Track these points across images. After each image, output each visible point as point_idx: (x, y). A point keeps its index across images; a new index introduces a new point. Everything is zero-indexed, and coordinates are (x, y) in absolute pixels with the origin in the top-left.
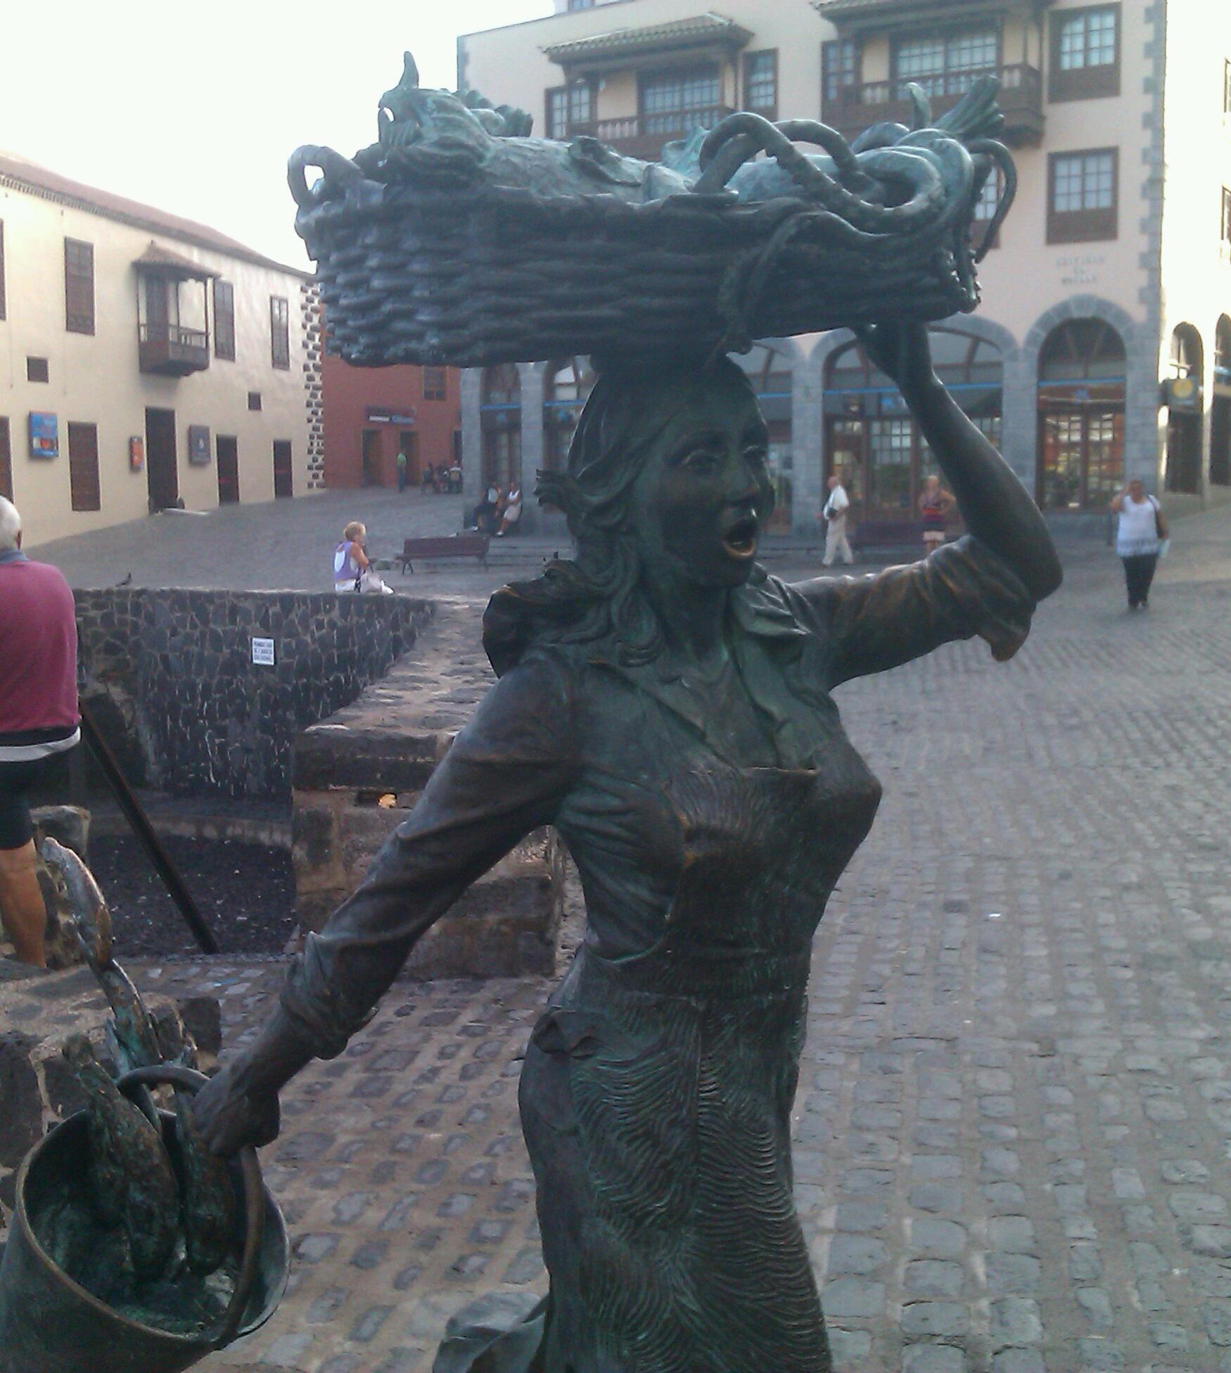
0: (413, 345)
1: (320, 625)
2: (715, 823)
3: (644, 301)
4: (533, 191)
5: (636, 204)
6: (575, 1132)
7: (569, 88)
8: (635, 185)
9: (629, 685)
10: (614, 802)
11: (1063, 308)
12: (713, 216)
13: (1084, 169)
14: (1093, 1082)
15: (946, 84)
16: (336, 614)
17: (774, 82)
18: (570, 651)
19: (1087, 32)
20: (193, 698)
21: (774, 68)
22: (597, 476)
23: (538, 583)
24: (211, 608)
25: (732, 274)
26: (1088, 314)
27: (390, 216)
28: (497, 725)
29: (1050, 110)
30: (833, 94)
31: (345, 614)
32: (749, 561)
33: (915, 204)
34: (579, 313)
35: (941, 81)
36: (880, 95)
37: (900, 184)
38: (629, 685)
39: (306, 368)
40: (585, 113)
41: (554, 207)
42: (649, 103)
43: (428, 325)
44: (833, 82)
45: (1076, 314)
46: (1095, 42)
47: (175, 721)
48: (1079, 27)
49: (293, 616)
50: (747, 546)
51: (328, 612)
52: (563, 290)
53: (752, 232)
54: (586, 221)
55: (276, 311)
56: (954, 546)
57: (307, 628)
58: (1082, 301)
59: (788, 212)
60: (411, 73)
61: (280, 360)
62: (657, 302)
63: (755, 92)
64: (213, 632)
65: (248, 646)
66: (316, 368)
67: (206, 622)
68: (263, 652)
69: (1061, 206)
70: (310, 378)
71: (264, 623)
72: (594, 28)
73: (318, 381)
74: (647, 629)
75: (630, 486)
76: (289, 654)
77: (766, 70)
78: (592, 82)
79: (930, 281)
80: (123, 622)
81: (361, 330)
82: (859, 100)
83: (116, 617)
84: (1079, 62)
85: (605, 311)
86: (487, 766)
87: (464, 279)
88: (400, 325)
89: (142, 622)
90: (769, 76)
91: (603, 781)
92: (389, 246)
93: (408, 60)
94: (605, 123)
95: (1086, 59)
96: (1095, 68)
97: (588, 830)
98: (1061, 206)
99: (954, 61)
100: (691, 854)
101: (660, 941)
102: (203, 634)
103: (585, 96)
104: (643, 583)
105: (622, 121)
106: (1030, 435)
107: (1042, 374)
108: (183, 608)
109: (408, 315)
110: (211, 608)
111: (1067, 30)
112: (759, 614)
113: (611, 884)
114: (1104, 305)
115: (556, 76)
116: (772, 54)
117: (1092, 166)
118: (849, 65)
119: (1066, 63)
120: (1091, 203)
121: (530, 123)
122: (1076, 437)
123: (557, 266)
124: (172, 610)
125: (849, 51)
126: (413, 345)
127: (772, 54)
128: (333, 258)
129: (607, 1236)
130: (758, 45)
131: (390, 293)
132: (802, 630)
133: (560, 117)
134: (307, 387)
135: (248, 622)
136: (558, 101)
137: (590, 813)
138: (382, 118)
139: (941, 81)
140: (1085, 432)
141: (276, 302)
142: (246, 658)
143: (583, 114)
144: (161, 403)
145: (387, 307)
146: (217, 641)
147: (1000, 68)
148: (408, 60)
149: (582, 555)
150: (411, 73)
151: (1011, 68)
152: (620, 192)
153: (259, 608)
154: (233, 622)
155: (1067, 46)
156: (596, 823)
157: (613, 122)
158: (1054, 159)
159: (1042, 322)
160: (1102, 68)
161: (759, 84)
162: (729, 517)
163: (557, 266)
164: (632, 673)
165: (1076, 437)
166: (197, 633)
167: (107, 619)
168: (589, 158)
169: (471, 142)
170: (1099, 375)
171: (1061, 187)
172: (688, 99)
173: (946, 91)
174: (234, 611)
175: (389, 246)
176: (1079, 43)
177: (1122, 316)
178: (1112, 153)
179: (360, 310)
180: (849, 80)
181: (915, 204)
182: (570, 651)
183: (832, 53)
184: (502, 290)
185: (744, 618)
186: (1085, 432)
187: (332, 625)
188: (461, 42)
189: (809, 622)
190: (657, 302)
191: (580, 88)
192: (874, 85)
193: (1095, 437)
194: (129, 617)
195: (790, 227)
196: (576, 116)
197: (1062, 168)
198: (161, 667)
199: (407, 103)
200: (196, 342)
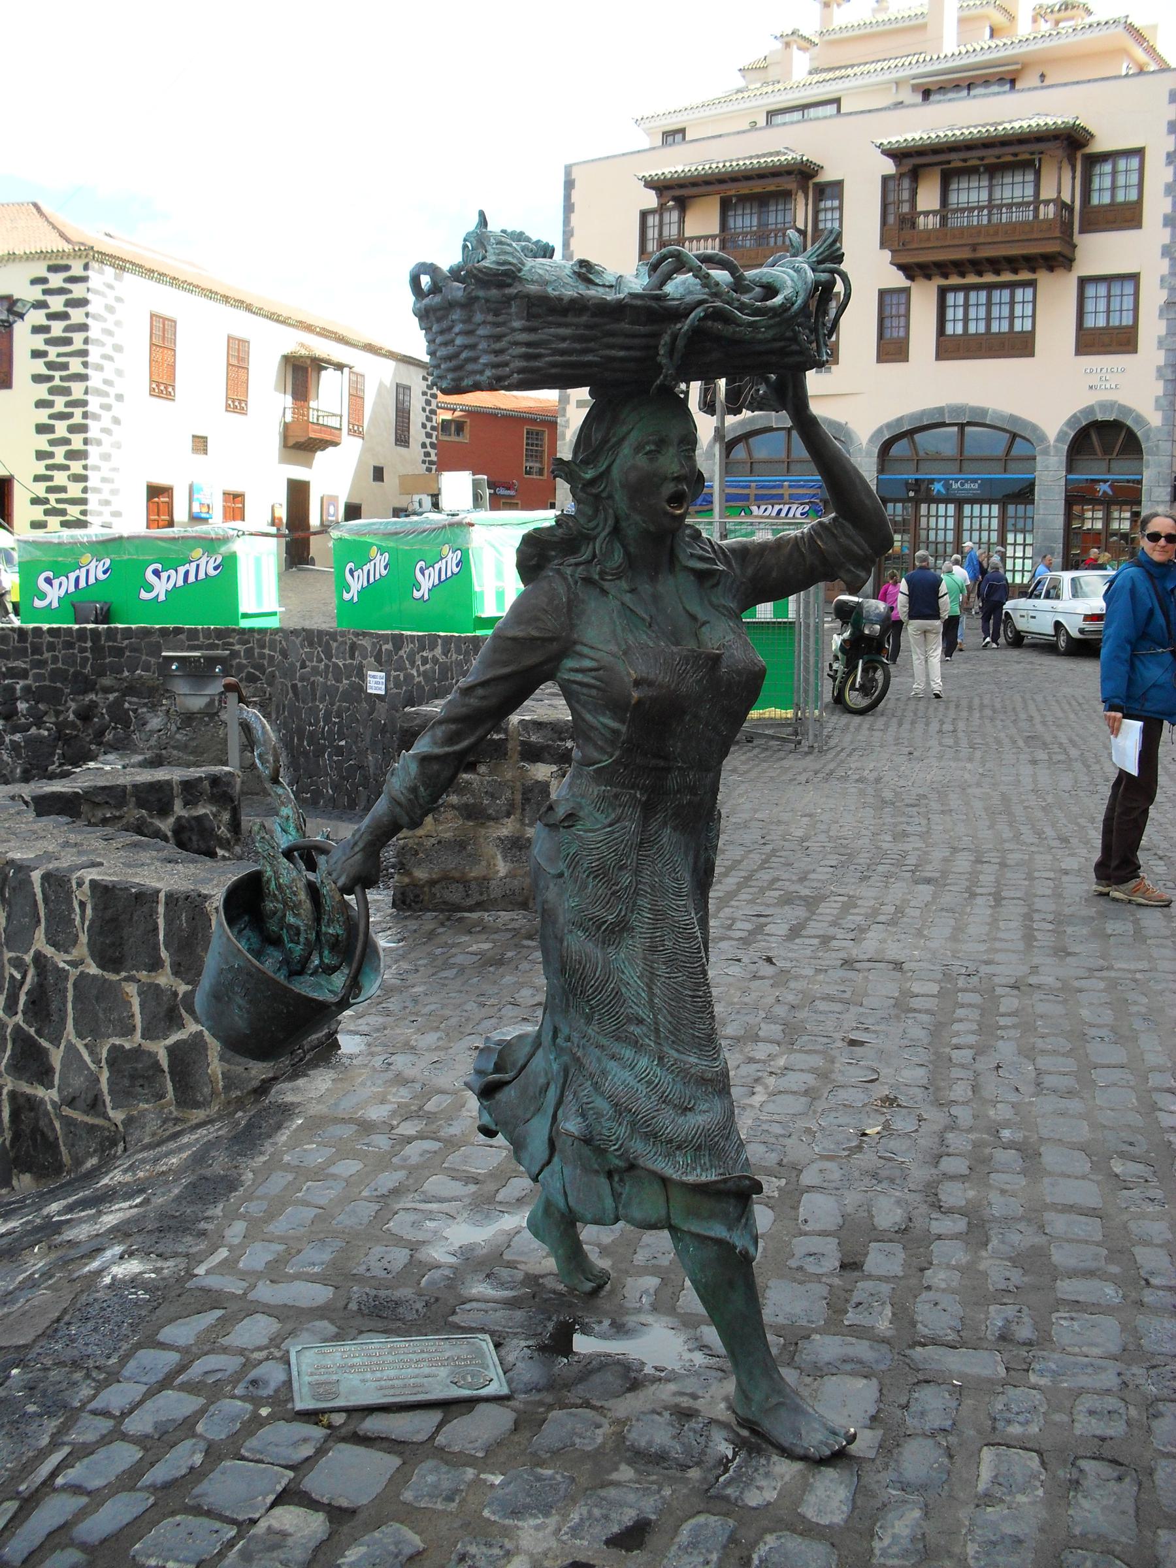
0: (478, 377)
1: (425, 661)
2: (652, 676)
3: (613, 353)
4: (550, 290)
5: (611, 296)
6: (561, 875)
7: (661, 209)
8: (611, 286)
9: (604, 592)
10: (587, 663)
11: (1090, 410)
12: (654, 304)
13: (1109, 291)
14: (999, 991)
15: (990, 214)
16: (438, 651)
17: (841, 208)
18: (569, 571)
19: (1114, 173)
20: (317, 721)
21: (840, 197)
22: (586, 462)
23: (551, 528)
24: (334, 645)
25: (666, 338)
26: (1111, 418)
27: (468, 304)
28: (519, 609)
29: (1078, 238)
30: (891, 219)
31: (446, 653)
32: (682, 517)
33: (778, 300)
34: (573, 358)
35: (985, 212)
36: (932, 222)
37: (771, 290)
38: (604, 592)
39: (424, 445)
40: (674, 230)
41: (560, 299)
42: (953, 198)
43: (486, 365)
44: (891, 209)
45: (1100, 417)
46: (1121, 180)
47: (301, 740)
48: (1107, 168)
49: (402, 653)
50: (679, 507)
51: (432, 650)
52: (564, 345)
53: (678, 313)
54: (577, 306)
55: (474, 1305)
56: (825, 520)
57: (413, 663)
58: (1104, 406)
59: (701, 303)
60: (483, 221)
61: (402, 439)
62: (622, 353)
63: (822, 216)
64: (336, 665)
65: (362, 677)
66: (433, 445)
67: (329, 657)
68: (376, 683)
69: (1089, 323)
70: (427, 454)
71: (378, 659)
72: (678, 163)
73: (434, 458)
74: (618, 557)
75: (609, 467)
76: (398, 685)
77: (832, 198)
78: (682, 204)
79: (794, 347)
80: (262, 656)
81: (449, 370)
82: (913, 225)
83: (257, 651)
84: (1106, 200)
85: (589, 358)
86: (514, 639)
87: (508, 338)
88: (470, 367)
89: (278, 657)
90: (836, 203)
91: (586, 650)
92: (468, 320)
93: (482, 215)
94: (691, 239)
95: (1113, 196)
96: (1121, 204)
97: (574, 682)
98: (1089, 323)
99: (997, 195)
100: (635, 695)
101: (617, 753)
102: (327, 666)
103: (675, 216)
104: (616, 531)
105: (706, 238)
106: (1059, 521)
107: (1070, 470)
108: (311, 645)
109: (475, 360)
110: (334, 645)
111: (1097, 170)
112: (692, 555)
113: (588, 717)
114: (1127, 411)
115: (651, 200)
116: (839, 184)
117: (1116, 289)
118: (906, 195)
119: (1095, 201)
120: (1115, 322)
121: (553, 250)
122: (1099, 525)
123: (562, 331)
124: (302, 647)
125: (906, 183)
126: (478, 377)
127: (839, 184)
128: (435, 328)
129: (577, 943)
130: (827, 176)
131: (466, 347)
132: (721, 567)
133: (652, 233)
134: (424, 462)
135: (365, 658)
136: (652, 220)
137: (577, 671)
138: (465, 247)
139: (985, 212)
140: (1107, 520)
141: (402, 390)
142: (361, 689)
143: (672, 231)
144: (299, 473)
145: (464, 355)
146: (338, 674)
147: (1037, 202)
148: (482, 215)
149: (578, 511)
150: (483, 221)
151: (1047, 202)
152: (600, 289)
153: (374, 644)
154: (352, 657)
155: (1096, 185)
156: (579, 677)
157: (698, 239)
158: (1083, 282)
159: (1071, 422)
160: (1126, 204)
161: (826, 210)
162: (668, 489)
163: (562, 331)
164: (606, 585)
165: (1099, 525)
166: (322, 666)
167: (249, 652)
168: (584, 270)
169: (514, 261)
170: (1121, 472)
171: (1089, 306)
172: (772, 220)
173: (989, 221)
174: (353, 647)
175: (468, 320)
176: (1107, 182)
177: (1139, 419)
178: (1134, 278)
179: (449, 358)
180: (906, 208)
181: (778, 300)
182: (569, 571)
183: (891, 185)
184: (528, 344)
185: (681, 556)
186: (1107, 520)
187: (435, 660)
188: (568, 170)
189: (728, 563)
190: (622, 353)
191: (670, 210)
192: (926, 214)
193: (1115, 525)
194: (266, 651)
195: (699, 312)
196: (666, 233)
197: (1090, 291)
198: (291, 695)
199: (479, 239)
200: (333, 422)
